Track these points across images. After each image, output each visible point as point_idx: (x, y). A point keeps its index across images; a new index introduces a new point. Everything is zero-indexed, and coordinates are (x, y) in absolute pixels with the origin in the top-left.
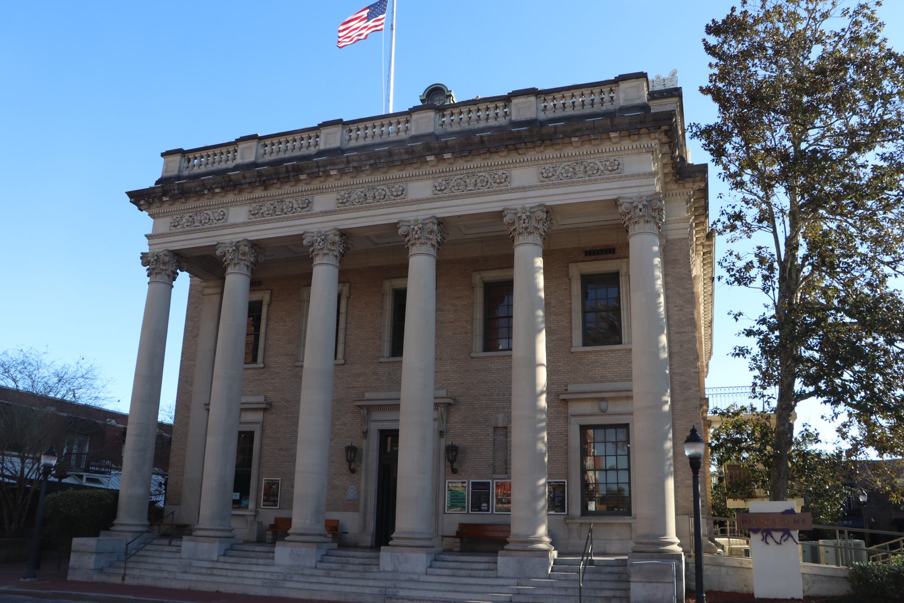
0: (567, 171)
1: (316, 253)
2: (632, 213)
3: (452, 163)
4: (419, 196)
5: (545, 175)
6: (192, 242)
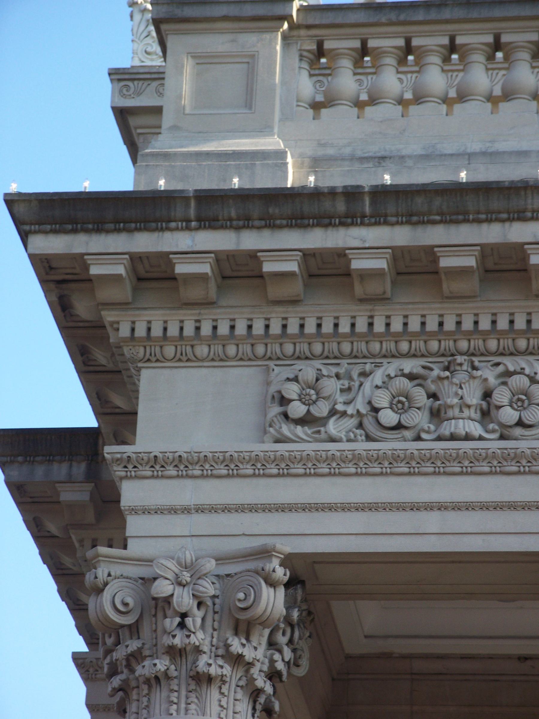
0: (402, 403)
1: (145, 669)
2: (146, 630)
3: (381, 299)
4: (202, 440)
5: (298, 409)
6: (432, 521)
